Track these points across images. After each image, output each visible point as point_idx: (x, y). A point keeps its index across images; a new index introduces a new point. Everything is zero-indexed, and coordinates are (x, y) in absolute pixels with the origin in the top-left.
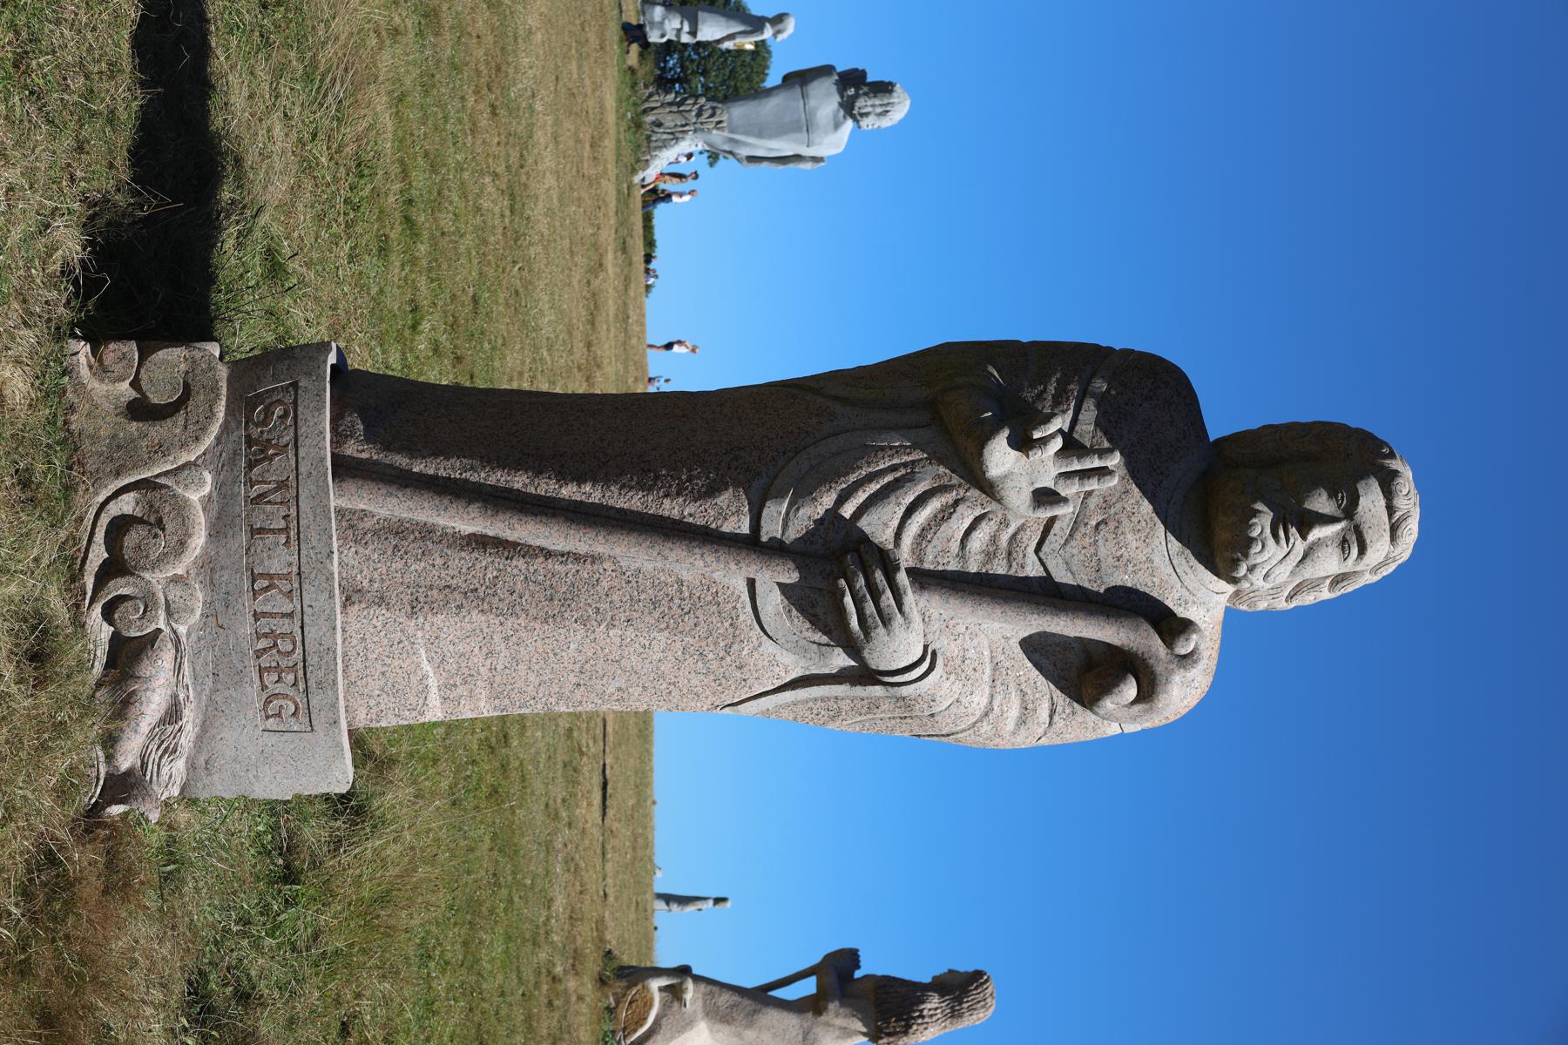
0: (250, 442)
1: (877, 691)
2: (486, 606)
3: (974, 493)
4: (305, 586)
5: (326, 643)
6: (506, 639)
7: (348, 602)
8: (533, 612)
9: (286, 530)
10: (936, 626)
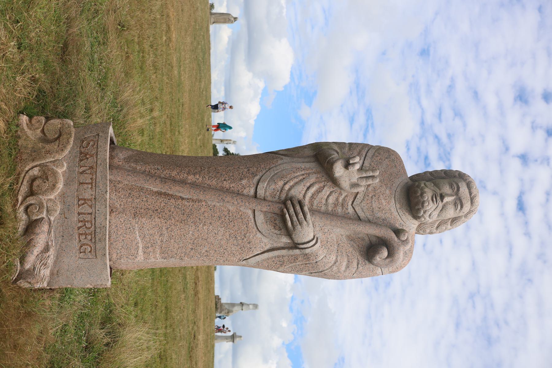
0: (81, 153)
1: (297, 252)
2: (160, 216)
3: (330, 184)
4: (97, 203)
5: (103, 224)
6: (167, 229)
7: (111, 211)
8: (177, 218)
9: (91, 184)
10: (318, 229)
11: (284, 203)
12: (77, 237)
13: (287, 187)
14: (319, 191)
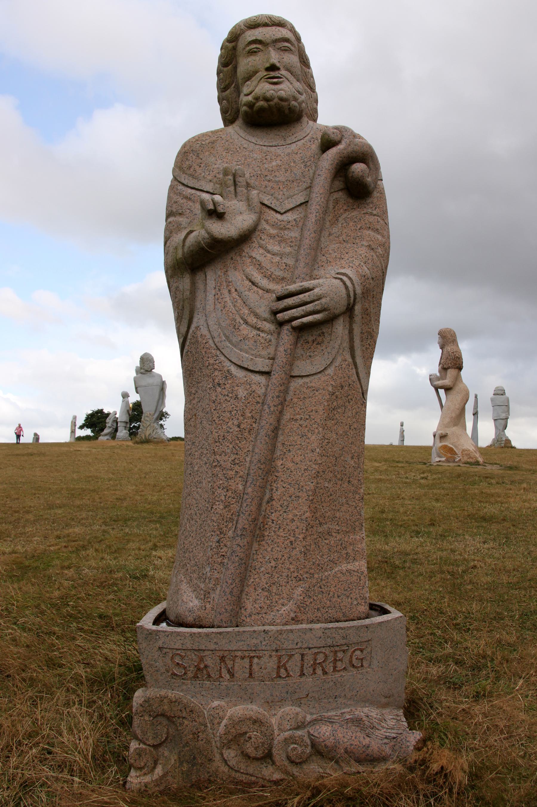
0: (196, 677)
1: (358, 308)
3: (246, 249)
4: (285, 646)
5: (320, 633)
11: (281, 324)
12: (338, 675)
13: (252, 320)
14: (259, 266)
